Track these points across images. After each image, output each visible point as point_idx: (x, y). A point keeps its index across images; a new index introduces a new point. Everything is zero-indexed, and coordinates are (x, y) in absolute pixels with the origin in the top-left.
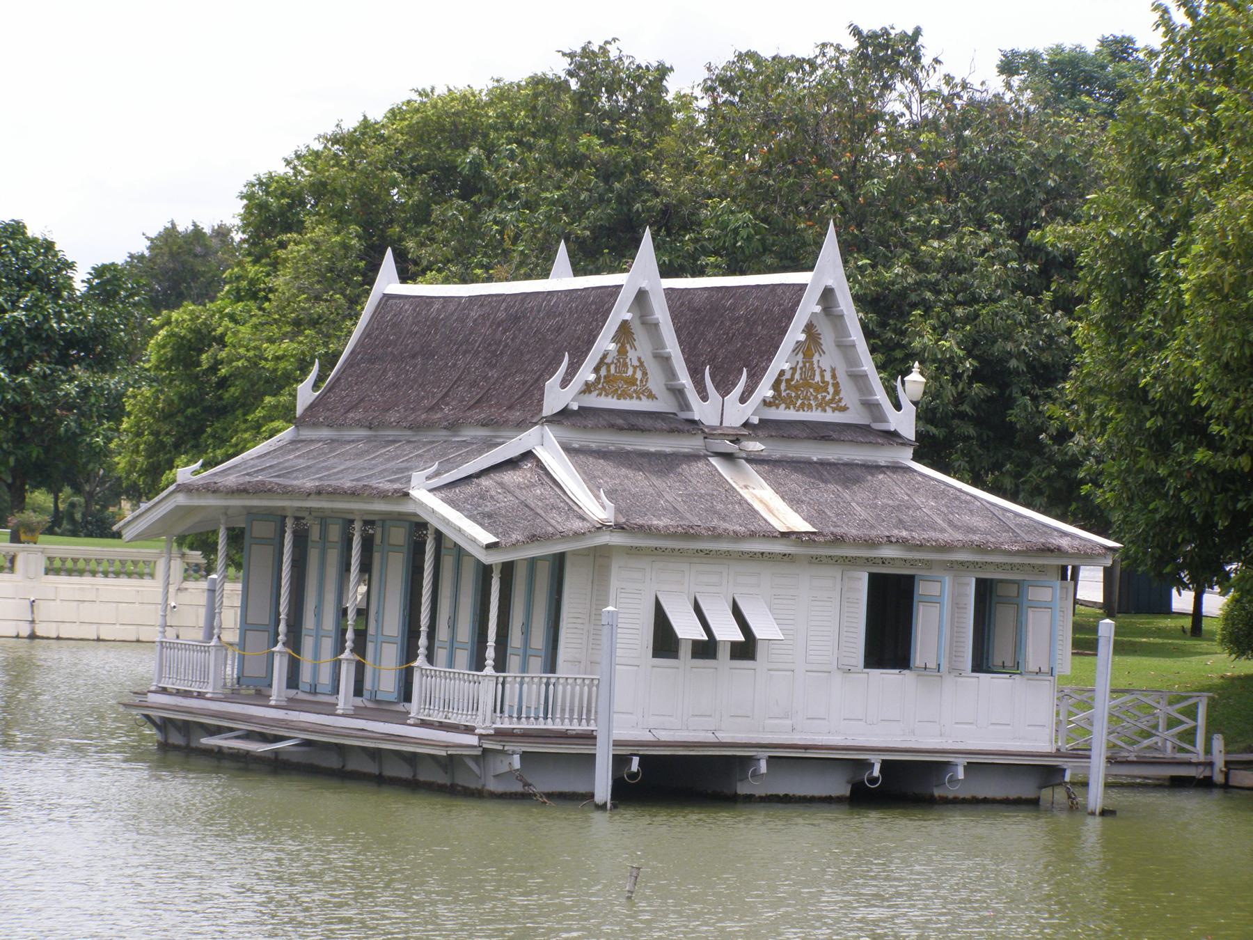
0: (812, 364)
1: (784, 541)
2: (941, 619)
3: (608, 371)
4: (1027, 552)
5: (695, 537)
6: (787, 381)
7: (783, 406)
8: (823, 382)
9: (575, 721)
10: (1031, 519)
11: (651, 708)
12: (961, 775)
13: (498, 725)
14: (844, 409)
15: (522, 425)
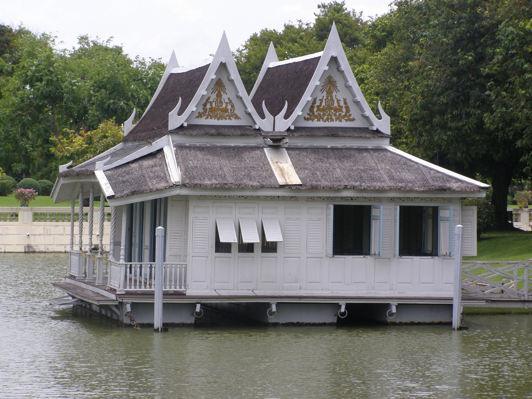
0: (332, 97)
1: (282, 190)
2: (385, 227)
3: (211, 105)
4: (430, 191)
5: (229, 189)
6: (317, 106)
7: (316, 120)
8: (339, 106)
9: (133, 286)
10: (443, 174)
11: (210, 279)
12: (394, 310)
13: (128, 289)
14: (353, 120)
15: (161, 135)
